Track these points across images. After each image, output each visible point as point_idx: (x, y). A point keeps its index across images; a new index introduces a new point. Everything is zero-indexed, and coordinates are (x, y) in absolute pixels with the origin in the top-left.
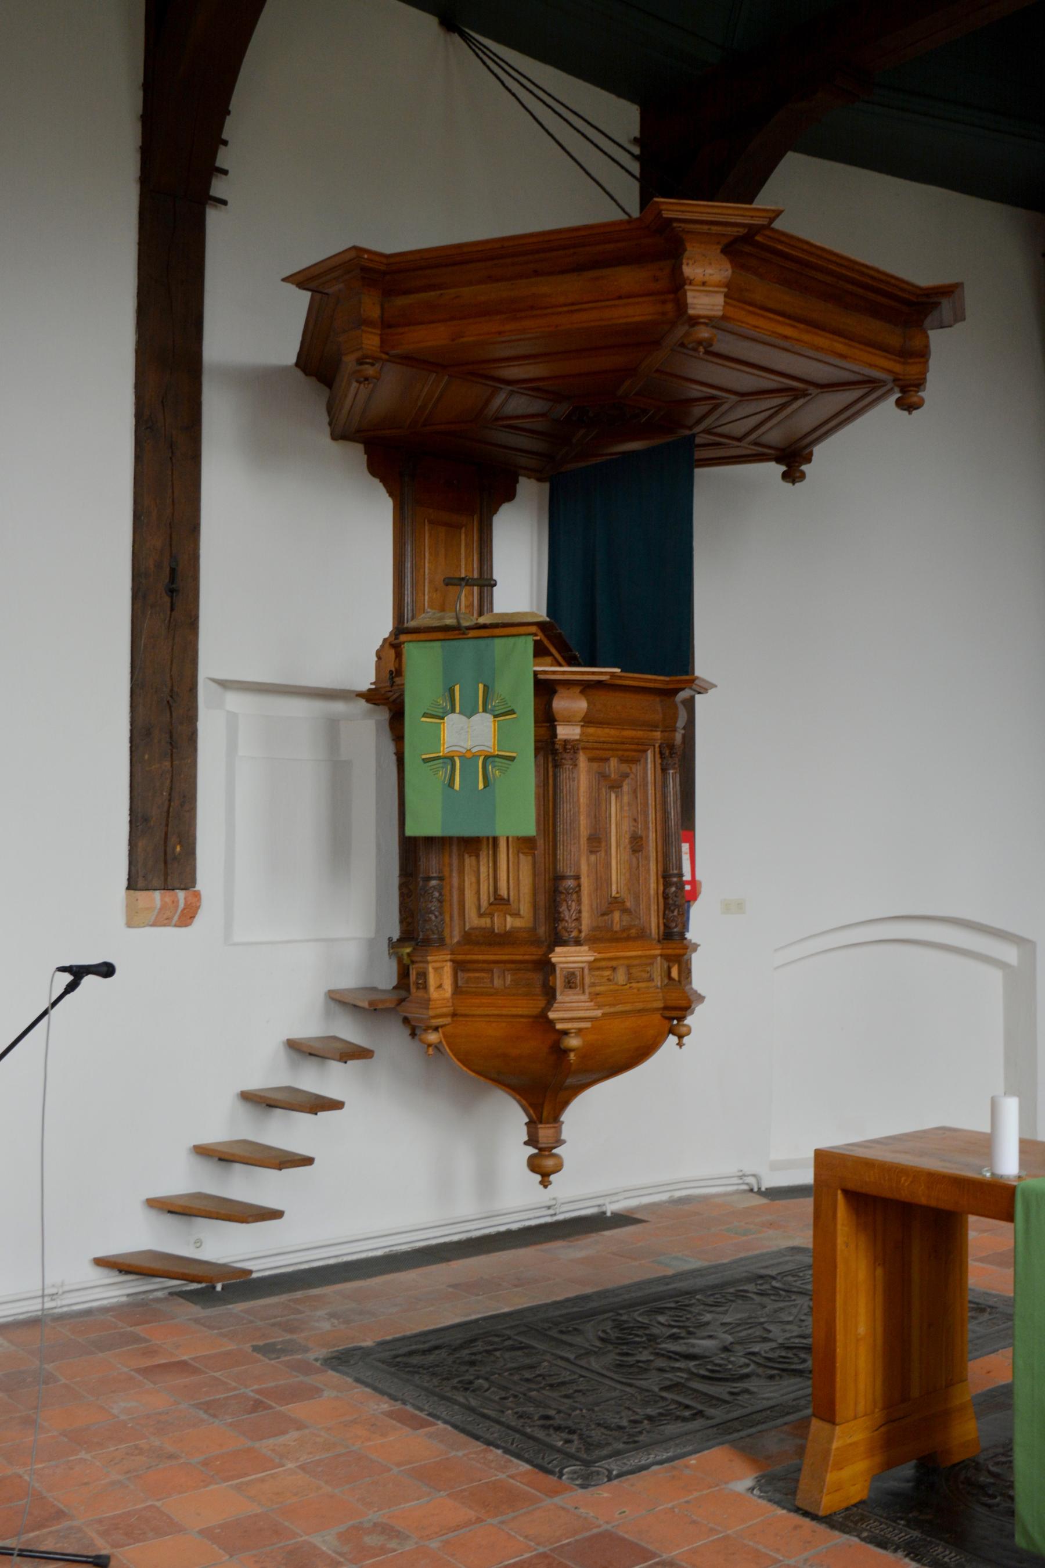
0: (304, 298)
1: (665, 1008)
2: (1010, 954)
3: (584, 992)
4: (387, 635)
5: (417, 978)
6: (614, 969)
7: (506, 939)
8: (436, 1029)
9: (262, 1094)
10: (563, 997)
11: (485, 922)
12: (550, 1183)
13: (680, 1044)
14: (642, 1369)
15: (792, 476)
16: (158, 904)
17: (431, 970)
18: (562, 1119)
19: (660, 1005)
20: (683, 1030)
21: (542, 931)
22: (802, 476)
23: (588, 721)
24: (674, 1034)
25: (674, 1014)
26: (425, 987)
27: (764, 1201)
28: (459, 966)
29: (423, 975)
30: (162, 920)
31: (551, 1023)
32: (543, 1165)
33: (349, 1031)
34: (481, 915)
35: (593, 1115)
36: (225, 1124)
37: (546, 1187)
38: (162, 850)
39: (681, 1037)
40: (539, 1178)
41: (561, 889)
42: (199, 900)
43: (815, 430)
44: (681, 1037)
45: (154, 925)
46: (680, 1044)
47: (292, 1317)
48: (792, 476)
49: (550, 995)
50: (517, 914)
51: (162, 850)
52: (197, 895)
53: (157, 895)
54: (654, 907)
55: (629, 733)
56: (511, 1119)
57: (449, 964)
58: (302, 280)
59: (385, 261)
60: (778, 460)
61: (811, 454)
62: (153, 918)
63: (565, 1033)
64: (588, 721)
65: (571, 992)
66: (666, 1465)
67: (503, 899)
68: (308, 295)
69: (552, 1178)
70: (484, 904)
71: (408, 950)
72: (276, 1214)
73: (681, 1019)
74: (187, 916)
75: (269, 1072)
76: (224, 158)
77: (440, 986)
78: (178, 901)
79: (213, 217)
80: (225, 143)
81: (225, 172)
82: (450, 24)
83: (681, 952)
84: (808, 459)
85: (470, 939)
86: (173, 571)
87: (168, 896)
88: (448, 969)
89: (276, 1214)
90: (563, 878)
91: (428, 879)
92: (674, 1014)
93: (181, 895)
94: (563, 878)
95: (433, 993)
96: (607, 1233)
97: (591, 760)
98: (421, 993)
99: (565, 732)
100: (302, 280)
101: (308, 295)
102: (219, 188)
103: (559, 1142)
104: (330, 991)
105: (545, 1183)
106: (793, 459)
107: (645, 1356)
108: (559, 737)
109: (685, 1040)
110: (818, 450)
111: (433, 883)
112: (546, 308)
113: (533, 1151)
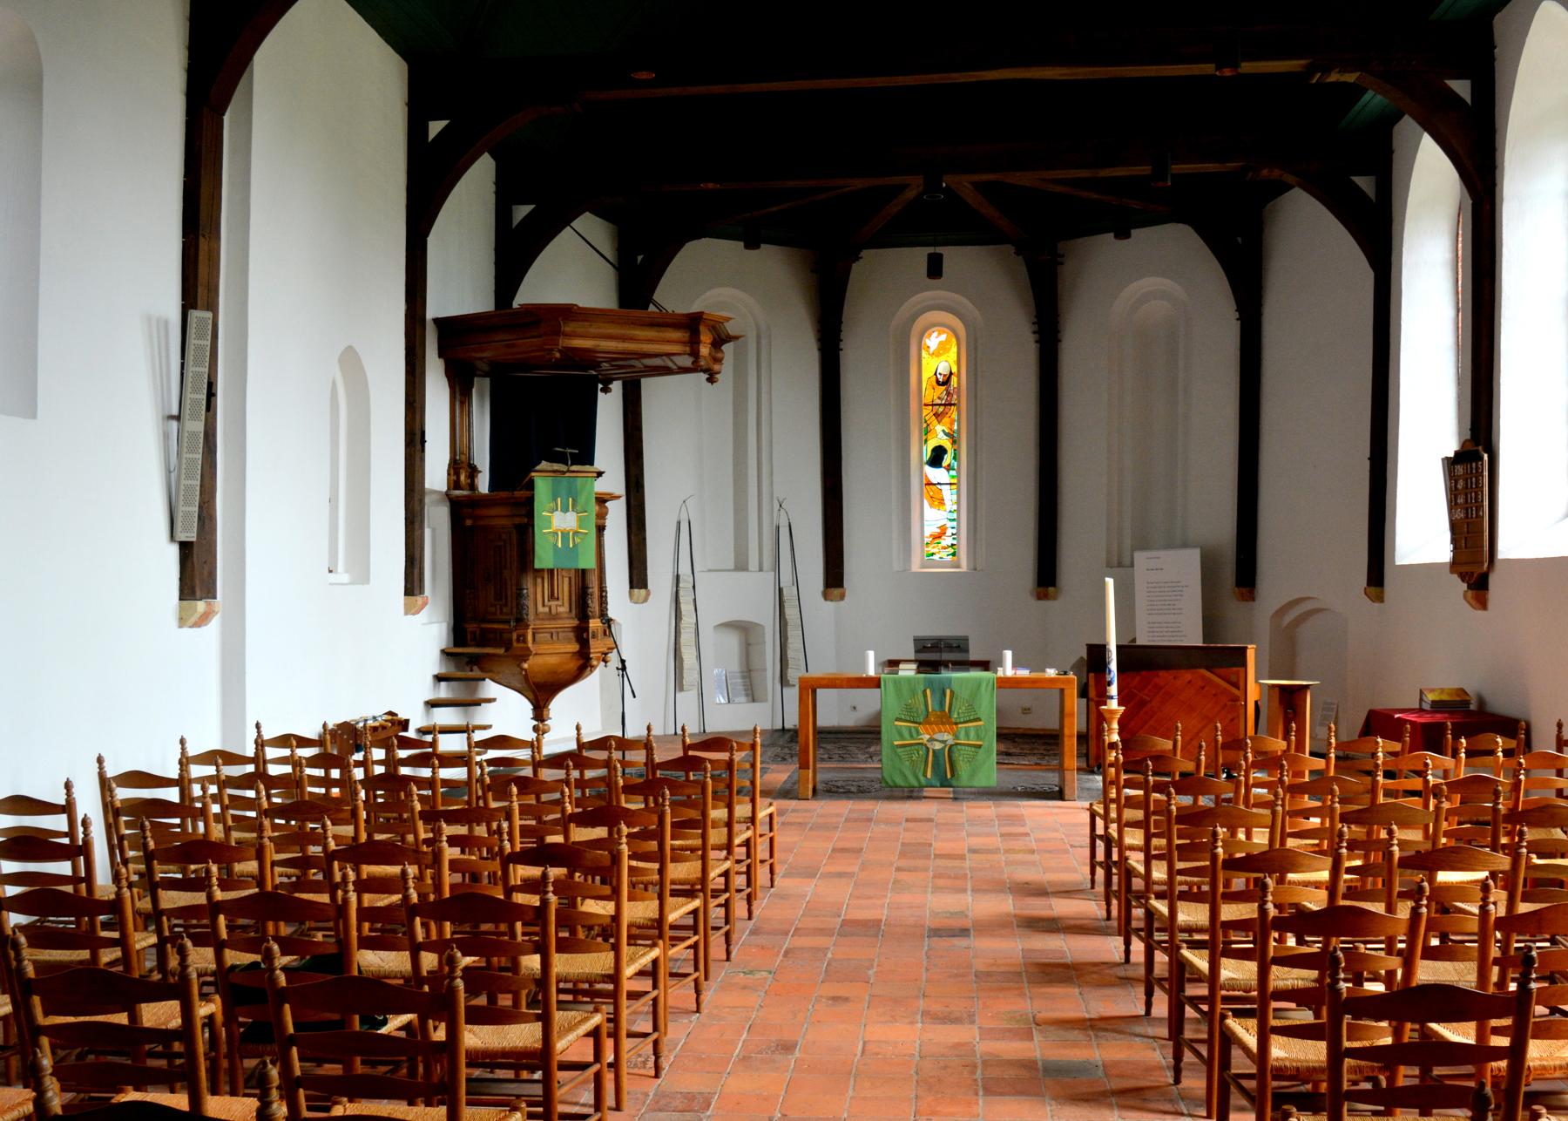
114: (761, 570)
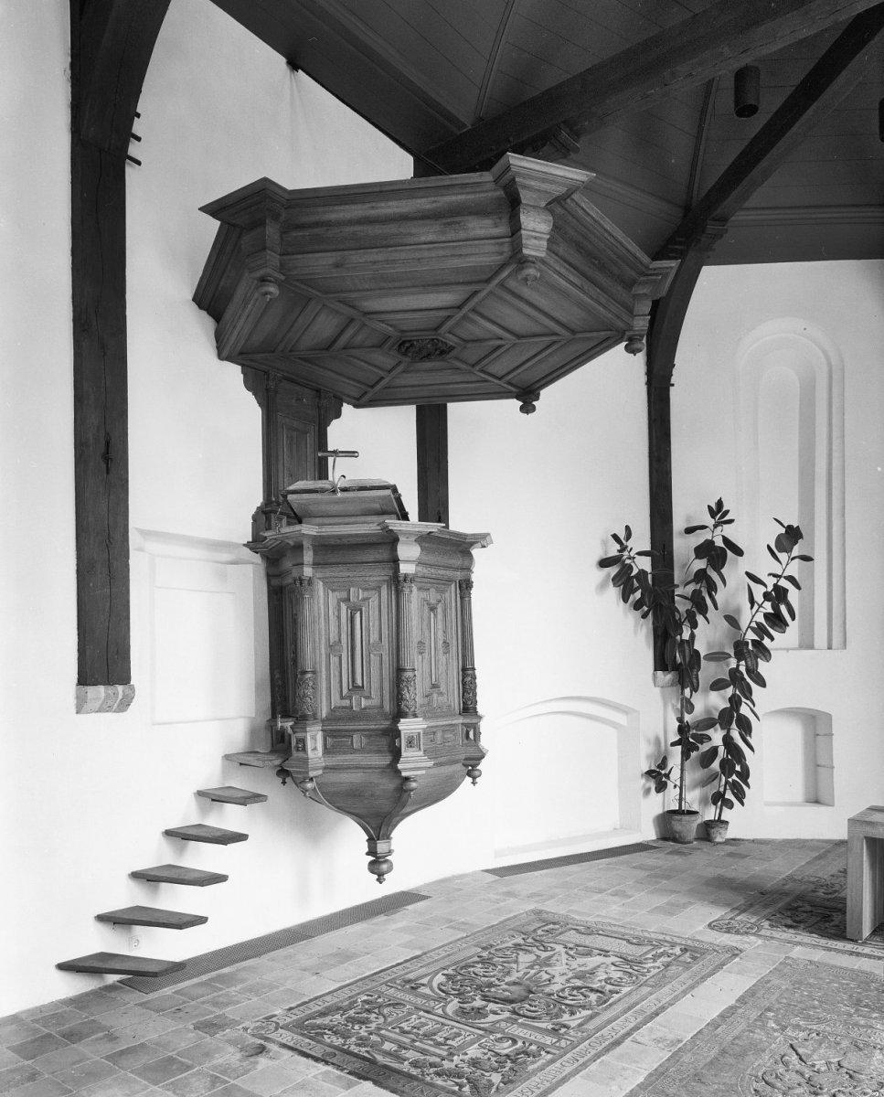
0: (214, 225)
1: (466, 759)
2: (621, 719)
3: (420, 749)
4: (259, 505)
5: (297, 743)
6: (434, 733)
7: (363, 715)
8: (311, 779)
9: (179, 831)
10: (406, 753)
11: (346, 703)
12: (384, 879)
13: (474, 783)
14: (479, 1012)
15: (527, 408)
16: (103, 695)
17: (309, 738)
18: (391, 836)
19: (463, 756)
20: (477, 773)
21: (387, 707)
22: (534, 409)
23: (419, 563)
24: (470, 776)
25: (471, 762)
26: (304, 749)
27: (493, 878)
28: (327, 734)
29: (303, 741)
30: (104, 708)
31: (399, 772)
32: (378, 865)
33: (241, 782)
34: (342, 698)
35: (408, 834)
36: (157, 854)
37: (381, 883)
38: (103, 658)
39: (474, 778)
40: (376, 877)
41: (403, 678)
42: (134, 692)
43: (538, 381)
44: (474, 778)
45: (99, 711)
46: (474, 783)
47: (215, 994)
48: (527, 408)
49: (396, 754)
50: (368, 698)
51: (103, 658)
52: (133, 689)
53: (101, 689)
54: (456, 693)
55: (442, 572)
56: (352, 836)
57: (320, 733)
58: (213, 209)
59: (287, 196)
60: (518, 398)
61: (539, 394)
62: (98, 706)
63: (407, 779)
64: (419, 563)
65: (411, 749)
66: (327, 991)
67: (359, 687)
68: (217, 224)
69: (386, 876)
70: (345, 691)
71: (291, 724)
72: (201, 920)
73: (474, 766)
74: (125, 704)
75: (185, 813)
76: (138, 127)
77: (315, 749)
78: (118, 694)
79: (131, 172)
80: (138, 116)
81: (139, 139)
82: (294, 65)
83: (474, 721)
84: (537, 398)
85: (334, 716)
86: (108, 444)
87: (110, 690)
88: (320, 736)
89: (201, 920)
90: (404, 670)
91: (306, 672)
92: (471, 762)
93: (120, 688)
94: (404, 670)
95: (310, 754)
96: (409, 907)
97: (419, 589)
98: (301, 754)
99: (405, 568)
100: (213, 209)
101: (217, 224)
102: (134, 149)
103: (390, 852)
104: (225, 755)
105: (380, 880)
106: (527, 397)
107: (478, 1003)
108: (401, 572)
109: (478, 780)
110: (543, 393)
111: (309, 675)
112: (406, 245)
113: (371, 858)
114: (830, 648)
